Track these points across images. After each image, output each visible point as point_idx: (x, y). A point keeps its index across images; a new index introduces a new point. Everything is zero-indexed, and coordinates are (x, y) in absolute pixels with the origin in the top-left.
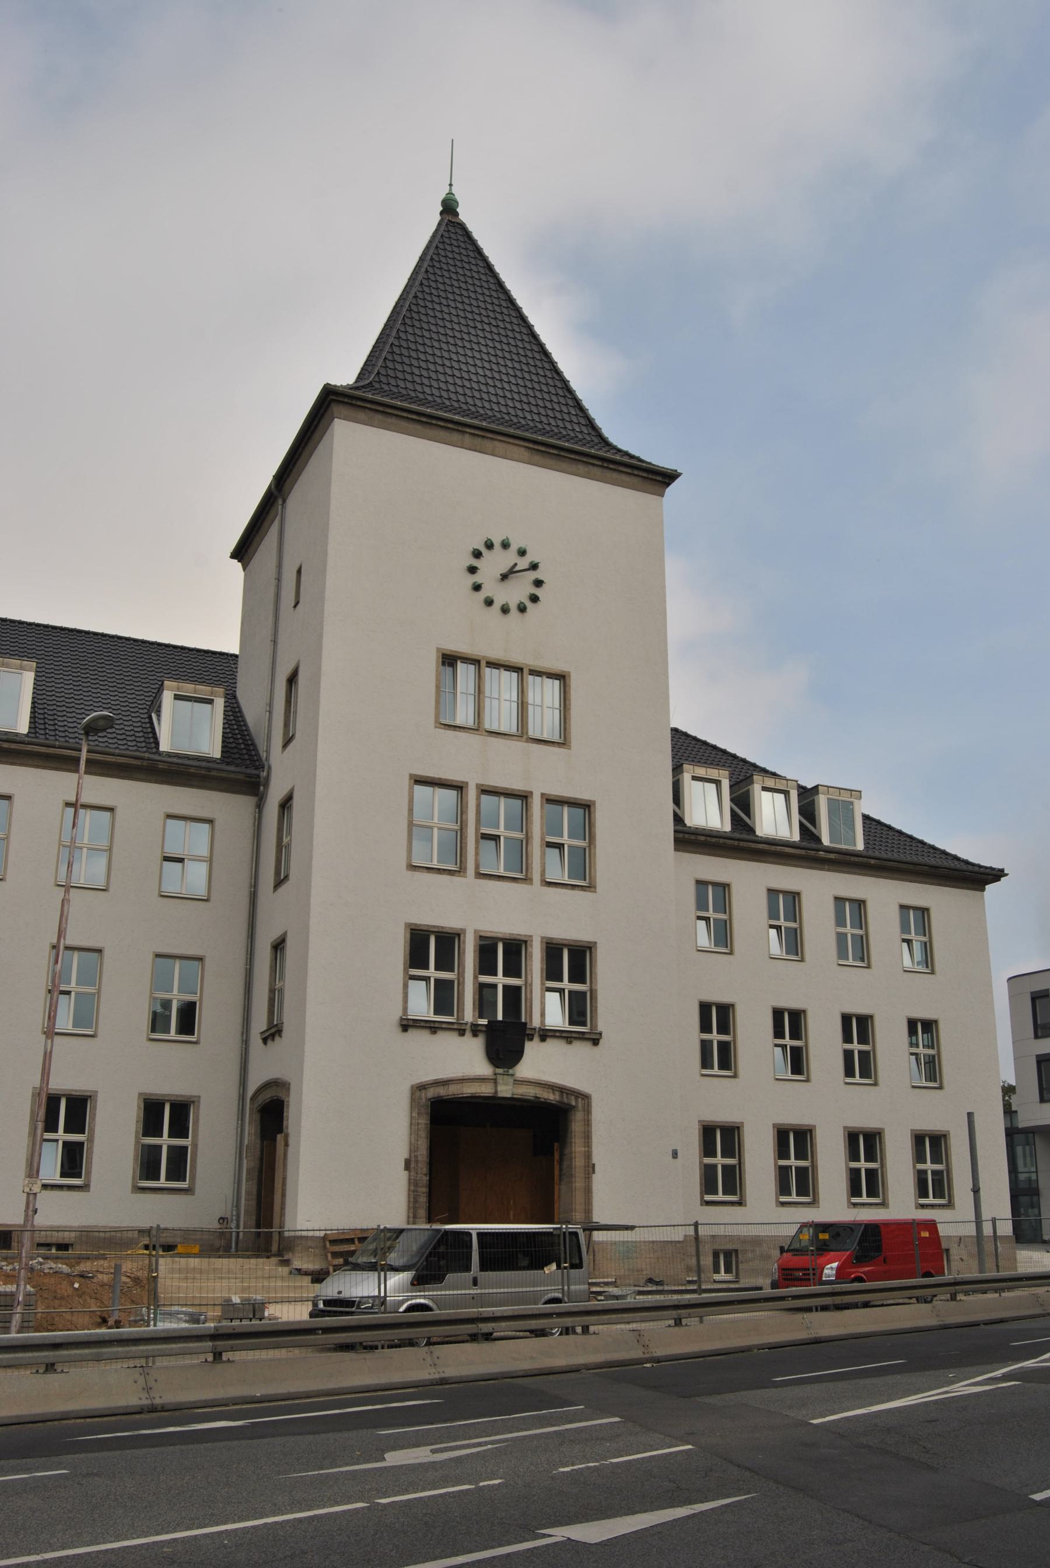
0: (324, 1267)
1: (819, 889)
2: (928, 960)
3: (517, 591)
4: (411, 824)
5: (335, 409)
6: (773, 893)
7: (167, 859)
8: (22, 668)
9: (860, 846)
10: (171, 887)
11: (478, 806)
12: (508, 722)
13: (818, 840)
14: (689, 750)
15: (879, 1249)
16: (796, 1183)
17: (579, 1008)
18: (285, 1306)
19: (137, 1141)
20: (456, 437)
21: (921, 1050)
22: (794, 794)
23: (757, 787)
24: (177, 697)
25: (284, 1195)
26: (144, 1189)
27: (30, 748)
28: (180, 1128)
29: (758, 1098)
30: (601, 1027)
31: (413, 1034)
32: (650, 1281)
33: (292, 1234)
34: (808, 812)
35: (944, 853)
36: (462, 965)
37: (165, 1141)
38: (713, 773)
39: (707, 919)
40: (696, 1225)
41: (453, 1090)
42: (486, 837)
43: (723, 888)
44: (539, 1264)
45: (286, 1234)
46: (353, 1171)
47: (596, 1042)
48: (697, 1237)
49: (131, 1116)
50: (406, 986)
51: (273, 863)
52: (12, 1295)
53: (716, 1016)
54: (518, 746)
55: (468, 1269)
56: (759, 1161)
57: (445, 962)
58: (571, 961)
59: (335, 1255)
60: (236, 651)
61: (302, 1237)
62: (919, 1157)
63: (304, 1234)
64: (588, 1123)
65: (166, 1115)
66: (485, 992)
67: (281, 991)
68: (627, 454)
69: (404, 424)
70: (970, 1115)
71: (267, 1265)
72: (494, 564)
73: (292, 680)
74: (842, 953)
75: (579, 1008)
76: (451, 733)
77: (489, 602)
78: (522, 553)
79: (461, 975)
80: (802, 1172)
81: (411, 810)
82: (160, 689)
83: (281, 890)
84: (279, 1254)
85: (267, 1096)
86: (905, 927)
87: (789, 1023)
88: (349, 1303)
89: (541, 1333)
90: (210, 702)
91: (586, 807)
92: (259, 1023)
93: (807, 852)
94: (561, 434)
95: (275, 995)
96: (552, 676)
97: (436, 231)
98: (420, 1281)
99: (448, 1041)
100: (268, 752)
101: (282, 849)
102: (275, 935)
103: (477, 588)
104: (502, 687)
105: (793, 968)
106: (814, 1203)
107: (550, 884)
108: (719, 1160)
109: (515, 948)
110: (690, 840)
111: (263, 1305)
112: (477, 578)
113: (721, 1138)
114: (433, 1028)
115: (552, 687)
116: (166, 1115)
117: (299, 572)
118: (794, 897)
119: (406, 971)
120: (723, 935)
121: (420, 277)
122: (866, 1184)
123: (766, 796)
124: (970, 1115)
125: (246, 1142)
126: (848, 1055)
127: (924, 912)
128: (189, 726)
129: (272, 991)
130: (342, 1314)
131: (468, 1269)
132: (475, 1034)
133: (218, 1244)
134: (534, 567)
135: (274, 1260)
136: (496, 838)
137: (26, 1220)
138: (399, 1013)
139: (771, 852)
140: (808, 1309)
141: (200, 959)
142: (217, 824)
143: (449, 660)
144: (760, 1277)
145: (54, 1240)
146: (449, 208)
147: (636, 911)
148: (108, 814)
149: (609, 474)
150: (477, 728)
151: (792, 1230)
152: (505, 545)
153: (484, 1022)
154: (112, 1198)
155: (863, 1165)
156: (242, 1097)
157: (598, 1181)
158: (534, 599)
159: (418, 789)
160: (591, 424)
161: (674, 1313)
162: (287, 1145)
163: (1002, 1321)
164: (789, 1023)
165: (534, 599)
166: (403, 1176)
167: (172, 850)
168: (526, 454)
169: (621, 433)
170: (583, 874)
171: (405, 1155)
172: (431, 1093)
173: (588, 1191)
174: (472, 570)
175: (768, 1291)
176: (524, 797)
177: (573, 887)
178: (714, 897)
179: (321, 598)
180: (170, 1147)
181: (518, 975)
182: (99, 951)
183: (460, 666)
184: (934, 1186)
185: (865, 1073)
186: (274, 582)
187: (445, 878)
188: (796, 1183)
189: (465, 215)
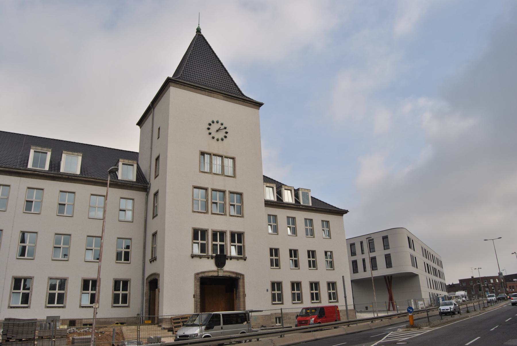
0: (171, 326)
1: (300, 216)
2: (329, 235)
3: (221, 135)
4: (193, 199)
5: (170, 84)
6: (306, 219)
7: (121, 210)
8: (78, 155)
9: (311, 205)
10: (122, 218)
11: (211, 194)
12: (219, 171)
13: (300, 203)
14: (267, 180)
15: (324, 314)
16: (298, 297)
17: (240, 250)
18: (166, 338)
19: (113, 293)
20: (204, 92)
21: (328, 259)
22: (293, 191)
23: (283, 189)
24: (123, 164)
25: (158, 306)
26: (48, 307)
27: (81, 178)
28: (125, 288)
29: (286, 274)
30: (246, 256)
31: (195, 259)
32: (262, 326)
33: (162, 317)
34: (297, 196)
35: (332, 206)
36: (208, 239)
37: (121, 292)
38: (272, 185)
39: (271, 225)
40: (281, 309)
41: (206, 275)
42: (214, 203)
43: (275, 216)
44: (242, 322)
45: (160, 317)
46: (179, 298)
47: (245, 260)
48: (282, 313)
49: (111, 285)
50: (192, 245)
51: (155, 211)
52: (90, 339)
53: (274, 252)
54: (222, 177)
55: (220, 324)
56: (287, 292)
57: (203, 238)
58: (238, 237)
59: (174, 323)
60: (138, 151)
61: (165, 318)
63: (166, 317)
64: (244, 282)
65: (121, 285)
66: (214, 246)
67: (155, 248)
68: (249, 98)
69: (189, 88)
70: (343, 277)
71: (155, 327)
73: (157, 159)
75: (240, 250)
76: (204, 174)
77: (213, 138)
78: (222, 124)
79: (208, 242)
81: (193, 195)
83: (155, 219)
84: (157, 324)
85: (152, 278)
86: (323, 227)
87: (294, 253)
88: (187, 336)
89: (240, 342)
90: (133, 165)
91: (241, 194)
92: (149, 257)
93: (297, 206)
94: (233, 94)
95: (154, 250)
97: (195, 37)
98: (207, 329)
99: (204, 261)
100: (150, 179)
101: (155, 207)
102: (153, 231)
103: (210, 134)
104: (217, 161)
105: (294, 238)
106: (302, 303)
107: (231, 216)
108: (276, 292)
109: (223, 234)
110: (268, 204)
111: (160, 338)
112: (210, 131)
113: (276, 286)
114: (200, 257)
115: (231, 161)
116: (89, 285)
117: (159, 129)
119: (192, 241)
120: (275, 229)
121: (192, 49)
122: (315, 297)
123: (286, 191)
124: (343, 277)
126: (309, 261)
127: (328, 222)
128: (126, 173)
129: (152, 248)
130: (185, 339)
131: (220, 324)
132: (212, 259)
133: (137, 321)
134: (225, 128)
135: (156, 325)
136: (216, 203)
137: (94, 316)
138: (191, 253)
139: (287, 206)
140: (310, 332)
141: (131, 239)
142: (135, 200)
143: (203, 154)
144: (292, 323)
145: (89, 323)
146: (198, 31)
147: (254, 224)
148: (73, 194)
149: (245, 103)
150: (211, 172)
151: (300, 310)
152: (217, 122)
153: (215, 255)
154: (106, 309)
155: (314, 292)
156: (143, 279)
157: (247, 299)
158: (226, 137)
159: (195, 189)
160: (239, 90)
161: (280, 334)
162: (159, 292)
163: (361, 332)
164: (294, 253)
166: (193, 299)
167: (122, 208)
169: (247, 93)
170: (240, 213)
172: (200, 276)
173: (244, 302)
174: (209, 129)
175: (294, 327)
176: (224, 192)
177: (238, 216)
178: (273, 219)
179: (167, 136)
180: (122, 294)
181: (223, 242)
182: (70, 235)
183: (206, 155)
184: (333, 296)
185: (314, 266)
186: (151, 132)
187: (203, 214)
188: (298, 297)
189: (203, 33)
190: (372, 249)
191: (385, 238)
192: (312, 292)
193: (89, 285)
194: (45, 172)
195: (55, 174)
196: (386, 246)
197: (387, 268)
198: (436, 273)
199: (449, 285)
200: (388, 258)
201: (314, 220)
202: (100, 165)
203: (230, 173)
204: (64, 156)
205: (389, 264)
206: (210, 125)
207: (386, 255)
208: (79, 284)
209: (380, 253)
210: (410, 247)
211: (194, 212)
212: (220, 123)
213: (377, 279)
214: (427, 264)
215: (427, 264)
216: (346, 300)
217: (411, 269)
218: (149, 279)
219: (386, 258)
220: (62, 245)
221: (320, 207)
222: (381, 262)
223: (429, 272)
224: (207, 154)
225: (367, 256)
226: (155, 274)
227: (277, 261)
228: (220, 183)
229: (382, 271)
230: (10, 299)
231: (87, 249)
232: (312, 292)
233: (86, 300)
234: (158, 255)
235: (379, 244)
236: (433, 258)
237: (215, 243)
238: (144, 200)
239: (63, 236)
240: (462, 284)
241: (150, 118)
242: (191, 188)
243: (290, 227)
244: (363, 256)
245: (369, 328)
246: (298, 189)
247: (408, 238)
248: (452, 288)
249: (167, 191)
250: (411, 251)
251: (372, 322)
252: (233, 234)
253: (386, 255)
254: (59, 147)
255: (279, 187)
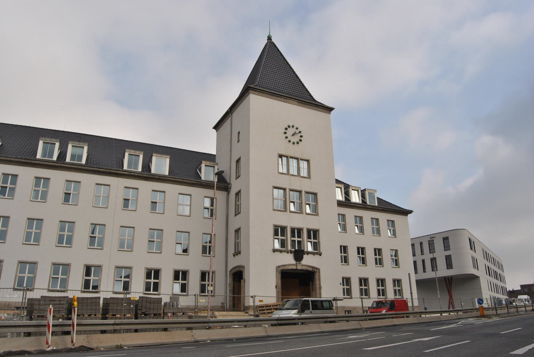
1: (367, 215)
2: (394, 234)
3: (296, 139)
4: (273, 199)
5: (250, 91)
9: (377, 205)
12: (295, 173)
13: (366, 203)
14: (338, 181)
16: (365, 293)
17: (316, 246)
20: (280, 99)
23: (351, 189)
24: (206, 166)
26: (202, 296)
29: (355, 271)
30: (321, 251)
38: (340, 186)
41: (286, 267)
46: (262, 287)
47: (320, 255)
53: (344, 249)
54: (298, 178)
57: (283, 234)
58: (314, 234)
59: (260, 310)
62: (395, 286)
64: (319, 276)
68: (320, 103)
69: (267, 95)
70: (409, 274)
72: (290, 131)
73: (238, 161)
74: (373, 233)
75: (316, 246)
78: (297, 129)
79: (287, 238)
80: (366, 290)
82: (201, 163)
84: (244, 311)
85: (236, 270)
87: (361, 251)
91: (315, 194)
92: (231, 250)
93: (363, 206)
96: (295, 158)
102: (237, 227)
103: (287, 138)
104: (293, 163)
109: (300, 231)
112: (286, 135)
114: (281, 251)
116: (180, 275)
117: (239, 133)
118: (361, 218)
122: (382, 293)
124: (409, 274)
125: (228, 283)
127: (393, 222)
131: (309, 309)
134: (300, 132)
139: (355, 206)
140: (389, 318)
142: (192, 196)
143: (281, 156)
146: (269, 38)
147: (326, 221)
149: (317, 108)
152: (293, 127)
155: (381, 288)
156: (226, 271)
157: (322, 290)
158: (301, 140)
159: (276, 191)
164: (361, 251)
165: (301, 140)
166: (275, 290)
168: (297, 103)
169: (318, 97)
170: (315, 211)
171: (275, 284)
172: (281, 268)
176: (300, 192)
183: (283, 158)
185: (380, 264)
186: (230, 136)
188: (365, 293)
189: (274, 40)
190: (432, 250)
191: (446, 240)
192: (378, 288)
193: (180, 275)
194: (139, 173)
195: (146, 175)
196: (447, 247)
197: (447, 269)
198: (497, 276)
199: (509, 291)
200: (448, 259)
201: (380, 220)
202: (186, 167)
203: (306, 175)
204: (154, 158)
205: (449, 265)
206: (286, 129)
207: (446, 256)
208: (171, 275)
209: (440, 254)
210: (471, 249)
211: (274, 210)
212: (295, 127)
213: (440, 279)
214: (488, 267)
215: (488, 267)
216: (411, 295)
217: (472, 271)
218: (233, 271)
219: (446, 259)
220: (155, 239)
221: (385, 207)
222: (441, 263)
223: (490, 275)
224: (285, 156)
225: (428, 257)
226: (240, 266)
227: (345, 257)
228: (297, 184)
229: (443, 272)
230: (114, 286)
231: (177, 243)
232: (378, 288)
233: (177, 288)
234: (242, 249)
235: (439, 245)
236: (494, 261)
237: (293, 239)
238: (225, 199)
239: (156, 231)
240: (523, 290)
241: (228, 122)
242: (272, 187)
243: (357, 226)
244: (423, 257)
245: (439, 320)
246: (365, 190)
247: (470, 239)
248: (513, 294)
249: (251, 190)
250: (472, 252)
251: (441, 315)
252: (309, 231)
253: (446, 256)
254: (149, 150)
255: (347, 188)
